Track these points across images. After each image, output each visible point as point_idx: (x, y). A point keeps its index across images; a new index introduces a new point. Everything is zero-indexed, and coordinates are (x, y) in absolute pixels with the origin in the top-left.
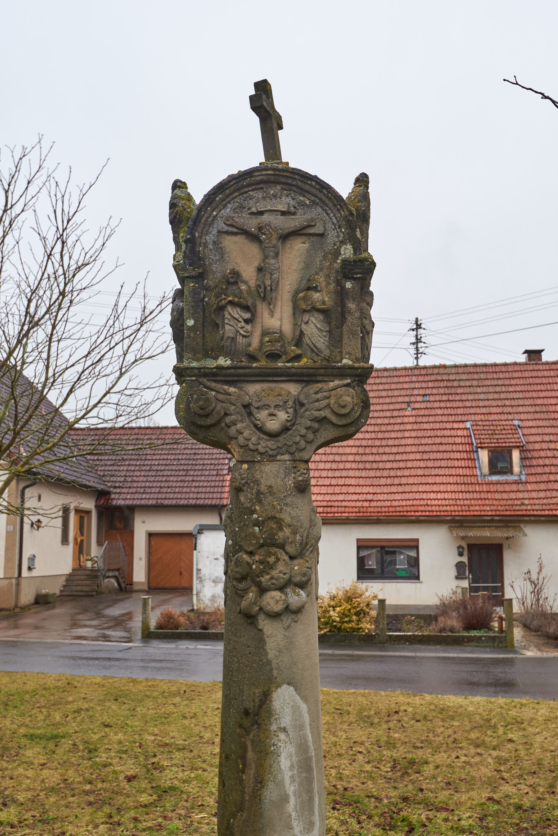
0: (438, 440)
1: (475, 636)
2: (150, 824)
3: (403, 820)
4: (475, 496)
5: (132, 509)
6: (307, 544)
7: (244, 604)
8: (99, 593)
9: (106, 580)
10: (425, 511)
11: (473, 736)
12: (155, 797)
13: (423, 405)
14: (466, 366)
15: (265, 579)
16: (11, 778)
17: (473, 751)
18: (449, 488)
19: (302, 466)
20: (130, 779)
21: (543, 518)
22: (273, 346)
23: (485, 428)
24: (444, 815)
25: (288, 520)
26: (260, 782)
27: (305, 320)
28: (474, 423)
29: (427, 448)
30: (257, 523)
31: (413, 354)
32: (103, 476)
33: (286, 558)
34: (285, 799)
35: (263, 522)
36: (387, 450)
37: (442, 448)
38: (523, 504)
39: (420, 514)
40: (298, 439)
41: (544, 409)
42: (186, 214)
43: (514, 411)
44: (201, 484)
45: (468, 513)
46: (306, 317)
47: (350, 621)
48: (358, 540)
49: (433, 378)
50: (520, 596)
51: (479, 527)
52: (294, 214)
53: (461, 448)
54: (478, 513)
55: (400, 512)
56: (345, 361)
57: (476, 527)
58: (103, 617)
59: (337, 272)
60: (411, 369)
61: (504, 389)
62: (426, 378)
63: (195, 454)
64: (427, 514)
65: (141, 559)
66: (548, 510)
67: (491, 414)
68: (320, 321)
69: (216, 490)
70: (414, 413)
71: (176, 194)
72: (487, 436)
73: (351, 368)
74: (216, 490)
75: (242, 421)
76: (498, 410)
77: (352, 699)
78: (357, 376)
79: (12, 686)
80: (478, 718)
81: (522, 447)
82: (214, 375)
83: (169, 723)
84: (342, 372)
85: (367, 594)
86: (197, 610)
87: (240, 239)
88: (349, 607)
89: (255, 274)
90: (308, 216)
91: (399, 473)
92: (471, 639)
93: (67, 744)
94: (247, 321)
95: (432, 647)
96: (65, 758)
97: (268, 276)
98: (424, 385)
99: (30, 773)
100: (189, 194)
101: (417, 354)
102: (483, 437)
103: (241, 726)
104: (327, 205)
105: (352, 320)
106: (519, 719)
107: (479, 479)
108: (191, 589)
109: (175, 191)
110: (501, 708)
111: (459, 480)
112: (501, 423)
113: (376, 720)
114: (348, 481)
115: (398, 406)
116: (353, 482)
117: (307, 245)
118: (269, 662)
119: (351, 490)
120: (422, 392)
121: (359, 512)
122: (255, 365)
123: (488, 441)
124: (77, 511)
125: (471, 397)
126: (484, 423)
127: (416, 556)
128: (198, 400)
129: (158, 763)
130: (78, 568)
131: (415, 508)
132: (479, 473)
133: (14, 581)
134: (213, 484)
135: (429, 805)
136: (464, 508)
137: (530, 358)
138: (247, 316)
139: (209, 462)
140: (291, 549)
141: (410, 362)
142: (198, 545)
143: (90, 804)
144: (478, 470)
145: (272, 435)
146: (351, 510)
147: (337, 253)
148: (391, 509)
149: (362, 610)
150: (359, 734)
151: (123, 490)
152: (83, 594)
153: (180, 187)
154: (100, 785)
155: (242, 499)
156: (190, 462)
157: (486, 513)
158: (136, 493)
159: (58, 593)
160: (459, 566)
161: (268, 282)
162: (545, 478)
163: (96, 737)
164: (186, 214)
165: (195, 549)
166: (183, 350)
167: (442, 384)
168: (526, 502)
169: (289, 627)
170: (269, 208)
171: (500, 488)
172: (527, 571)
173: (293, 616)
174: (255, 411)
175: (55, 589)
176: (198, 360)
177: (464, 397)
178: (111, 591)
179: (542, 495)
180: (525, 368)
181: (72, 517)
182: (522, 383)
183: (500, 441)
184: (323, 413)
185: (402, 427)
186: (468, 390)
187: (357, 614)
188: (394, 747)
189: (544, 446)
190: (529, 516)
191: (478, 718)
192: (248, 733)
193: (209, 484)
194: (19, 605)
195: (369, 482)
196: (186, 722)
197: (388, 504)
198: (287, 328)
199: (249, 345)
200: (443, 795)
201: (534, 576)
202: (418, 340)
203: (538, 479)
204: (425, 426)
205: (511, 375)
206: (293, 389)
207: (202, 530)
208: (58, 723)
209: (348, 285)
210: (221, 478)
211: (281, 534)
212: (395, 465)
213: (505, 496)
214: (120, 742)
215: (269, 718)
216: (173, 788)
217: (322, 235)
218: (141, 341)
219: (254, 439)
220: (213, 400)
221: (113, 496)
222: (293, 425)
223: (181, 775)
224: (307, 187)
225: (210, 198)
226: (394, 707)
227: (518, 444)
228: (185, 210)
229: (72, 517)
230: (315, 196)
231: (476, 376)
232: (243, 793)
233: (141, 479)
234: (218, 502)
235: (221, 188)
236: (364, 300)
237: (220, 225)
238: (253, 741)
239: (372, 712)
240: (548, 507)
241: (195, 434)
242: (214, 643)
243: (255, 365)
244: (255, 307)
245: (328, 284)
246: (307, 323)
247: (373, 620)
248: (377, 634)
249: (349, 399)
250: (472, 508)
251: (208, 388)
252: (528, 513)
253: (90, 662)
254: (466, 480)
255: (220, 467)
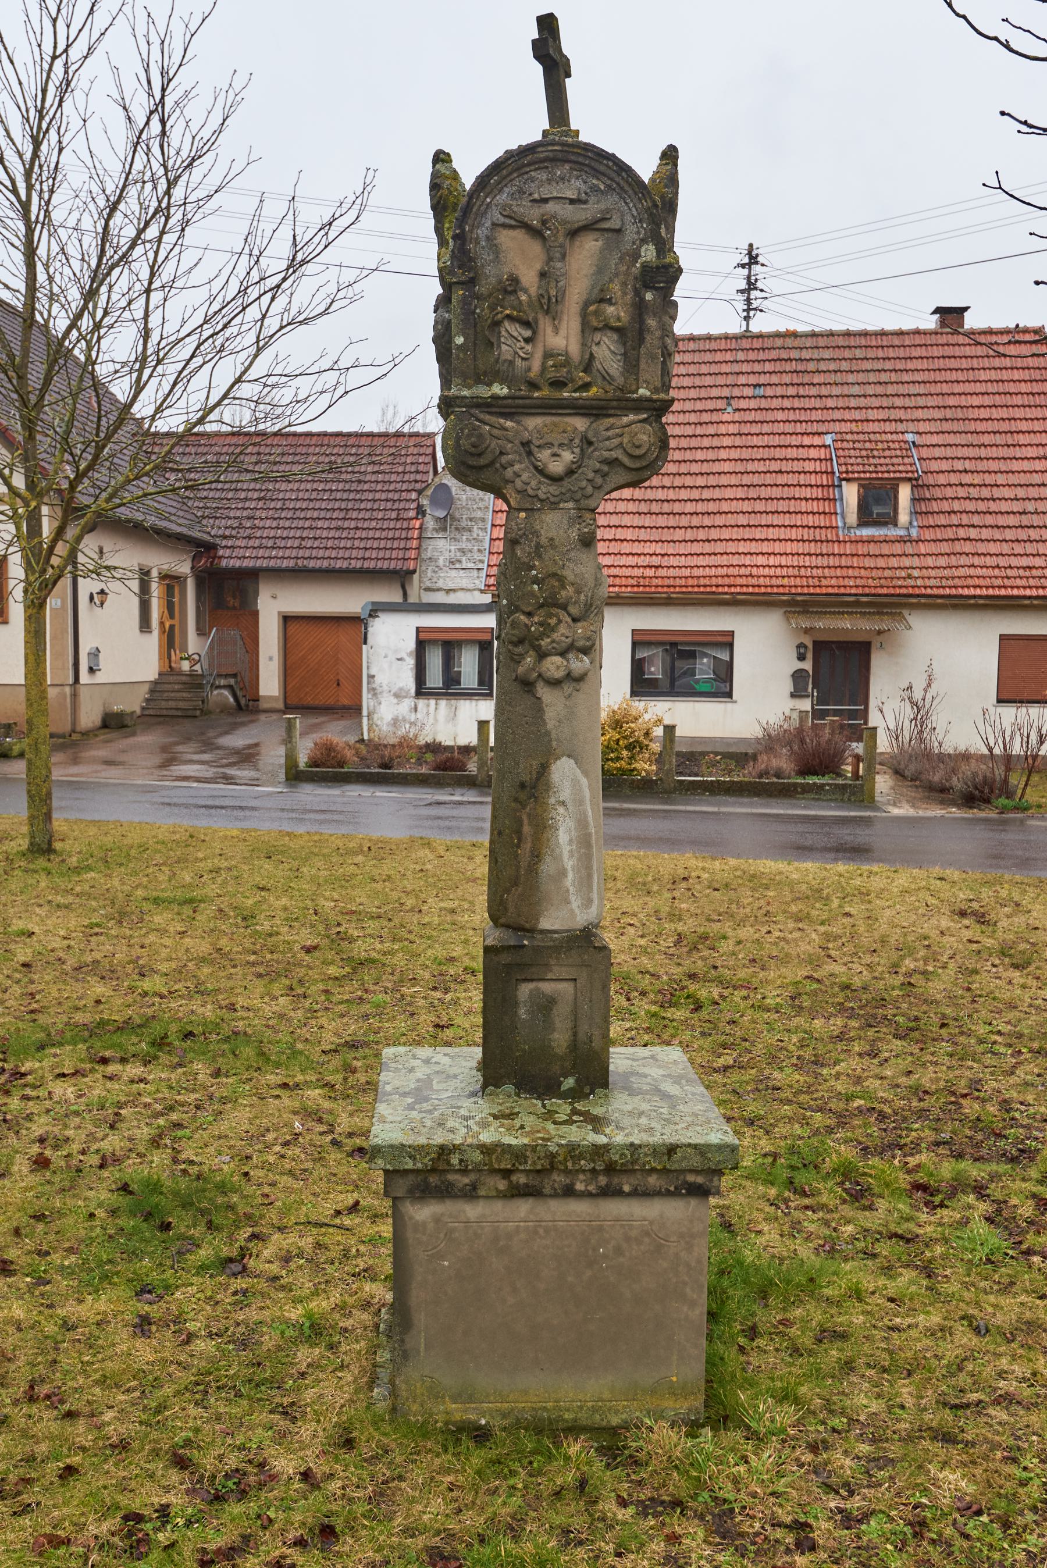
0: (775, 466)
1: (815, 784)
2: (346, 997)
3: (688, 997)
4: (832, 561)
5: (253, 575)
6: (591, 605)
7: (521, 670)
8: (205, 712)
9: (215, 692)
10: (747, 586)
11: (794, 908)
12: (348, 969)
13: (753, 404)
14: (831, 334)
15: (545, 643)
16: (142, 947)
17: (791, 925)
18: (789, 547)
19: (588, 516)
20: (309, 950)
21: (939, 601)
22: (557, 371)
23: (857, 445)
24: (744, 993)
25: (571, 577)
26: (537, 856)
27: (597, 340)
28: (839, 436)
29: (756, 479)
30: (536, 581)
31: (740, 311)
32: (203, 517)
33: (569, 620)
34: (563, 873)
35: (543, 579)
36: (689, 481)
37: (781, 479)
38: (910, 577)
39: (738, 590)
40: (584, 483)
41: (960, 414)
42: (452, 199)
43: (909, 417)
44: (371, 534)
45: (818, 590)
46: (597, 337)
47: (618, 759)
48: (634, 632)
49: (774, 355)
50: (892, 726)
51: (834, 613)
52: (585, 202)
53: (813, 479)
54: (836, 591)
55: (705, 586)
56: (641, 391)
57: (830, 613)
58: (218, 748)
59: (636, 278)
60: (736, 337)
61: (894, 377)
62: (762, 356)
63: (360, 482)
64: (751, 590)
65: (271, 659)
66: (950, 587)
67: (868, 421)
68: (614, 342)
69: (396, 544)
70: (737, 417)
71: (439, 171)
72: (859, 460)
73: (649, 400)
74: (396, 544)
75: (520, 462)
76: (882, 415)
77: (620, 862)
78: (655, 409)
79: (105, 839)
80: (804, 887)
81: (916, 479)
82: (488, 405)
83: (353, 887)
84: (638, 405)
85: (646, 717)
86: (370, 740)
87: (519, 234)
88: (617, 736)
89: (536, 279)
90: (602, 206)
91: (707, 521)
92: (806, 789)
93: (208, 911)
94: (527, 340)
95: (746, 800)
96: (212, 925)
97: (553, 284)
98: (757, 367)
99: (167, 942)
100: (455, 171)
101: (748, 310)
102: (852, 461)
103: (516, 800)
104: (626, 192)
105: (651, 340)
106: (864, 890)
107: (840, 533)
108: (358, 709)
109: (438, 166)
110: (840, 875)
111: (806, 534)
112: (884, 437)
113: (655, 888)
114: (620, 534)
115: (710, 405)
116: (629, 534)
117: (600, 243)
118: (548, 733)
119: (626, 548)
120: (752, 380)
121: (638, 586)
122: (536, 394)
123: (860, 468)
124: (164, 577)
125: (837, 390)
126: (856, 437)
127: (728, 659)
128: (469, 436)
129: (346, 933)
130: (169, 672)
131: (731, 581)
132: (840, 524)
133: (67, 690)
134: (391, 534)
135: (721, 982)
136: (811, 582)
137: (943, 323)
138: (528, 333)
139: (384, 496)
140: (574, 610)
141: (734, 326)
142: (369, 636)
143: (260, 976)
144: (839, 517)
145: (555, 479)
146: (624, 581)
147: (636, 255)
148: (690, 582)
149: (637, 741)
150: (628, 903)
151: (238, 543)
152: (179, 713)
153: (443, 161)
154: (269, 956)
155: (519, 553)
156: (352, 496)
157: (848, 591)
158: (260, 547)
159: (138, 712)
160: (798, 676)
161: (553, 292)
162: (950, 533)
163: (250, 902)
164: (452, 199)
165: (365, 643)
166: (449, 373)
167: (788, 367)
168: (916, 573)
169: (570, 695)
170: (555, 194)
171: (873, 549)
172: (907, 685)
173: (574, 684)
174: (535, 450)
175: (132, 704)
176: (469, 387)
177: (824, 391)
178: (225, 710)
179: (942, 561)
180: (933, 340)
181: (156, 589)
182: (925, 366)
183: (879, 468)
184: (614, 454)
185: (716, 442)
186: (832, 378)
187: (630, 747)
188: (680, 920)
189: (954, 479)
190: (918, 596)
191: (804, 887)
192: (524, 807)
193: (384, 534)
194: (78, 729)
195: (655, 535)
196: (379, 886)
197: (687, 572)
198: (574, 349)
199: (529, 370)
200: (742, 974)
201: (918, 695)
202: (751, 285)
203: (939, 534)
204: (756, 441)
205: (908, 352)
206: (580, 424)
207: (376, 611)
208: (190, 885)
209: (649, 296)
210: (405, 525)
211: (563, 593)
212: (700, 507)
213: (881, 562)
214: (285, 909)
215: (547, 791)
216: (371, 961)
217: (618, 231)
218: (288, 292)
219: (533, 483)
220: (488, 436)
221: (221, 552)
222: (579, 467)
223: (379, 946)
224: (602, 168)
225: (483, 181)
226: (681, 872)
227: (910, 475)
228: (451, 193)
229: (156, 589)
230: (612, 179)
231: (847, 354)
232: (518, 867)
233: (268, 523)
234: (399, 565)
235: (496, 168)
236: (666, 313)
237: (495, 215)
238: (529, 815)
239: (650, 878)
240: (950, 583)
241: (466, 476)
242: (402, 789)
243: (536, 394)
244: (536, 321)
245: (625, 294)
246: (598, 344)
247: (653, 758)
248: (661, 779)
249: (645, 438)
250: (824, 582)
251: (478, 420)
252: (917, 591)
253: (213, 811)
254: (818, 534)
255: (402, 505)
